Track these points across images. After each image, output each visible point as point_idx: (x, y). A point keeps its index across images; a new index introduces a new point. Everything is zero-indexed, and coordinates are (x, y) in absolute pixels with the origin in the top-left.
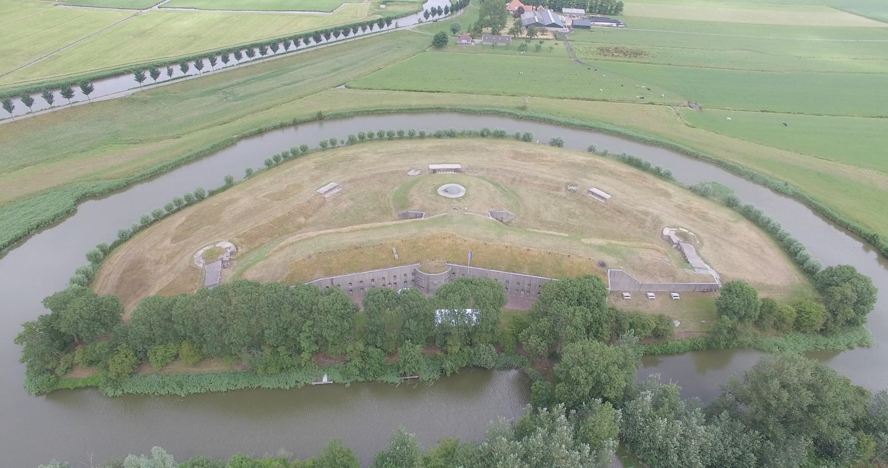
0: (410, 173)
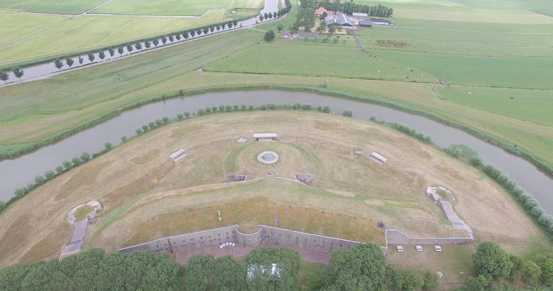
0: (240, 141)
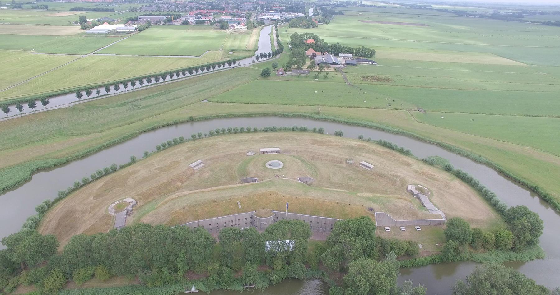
0: (248, 154)
